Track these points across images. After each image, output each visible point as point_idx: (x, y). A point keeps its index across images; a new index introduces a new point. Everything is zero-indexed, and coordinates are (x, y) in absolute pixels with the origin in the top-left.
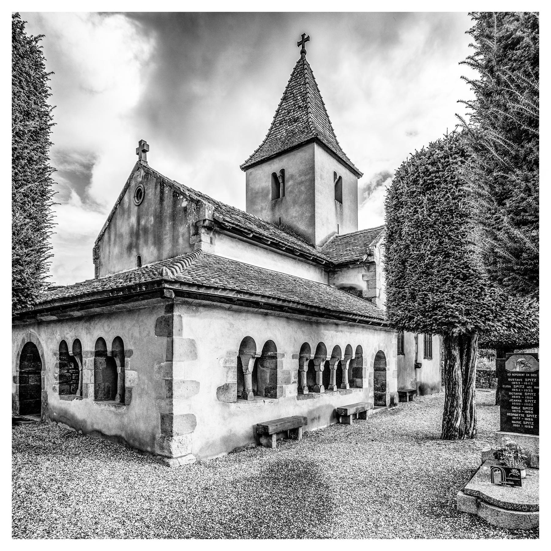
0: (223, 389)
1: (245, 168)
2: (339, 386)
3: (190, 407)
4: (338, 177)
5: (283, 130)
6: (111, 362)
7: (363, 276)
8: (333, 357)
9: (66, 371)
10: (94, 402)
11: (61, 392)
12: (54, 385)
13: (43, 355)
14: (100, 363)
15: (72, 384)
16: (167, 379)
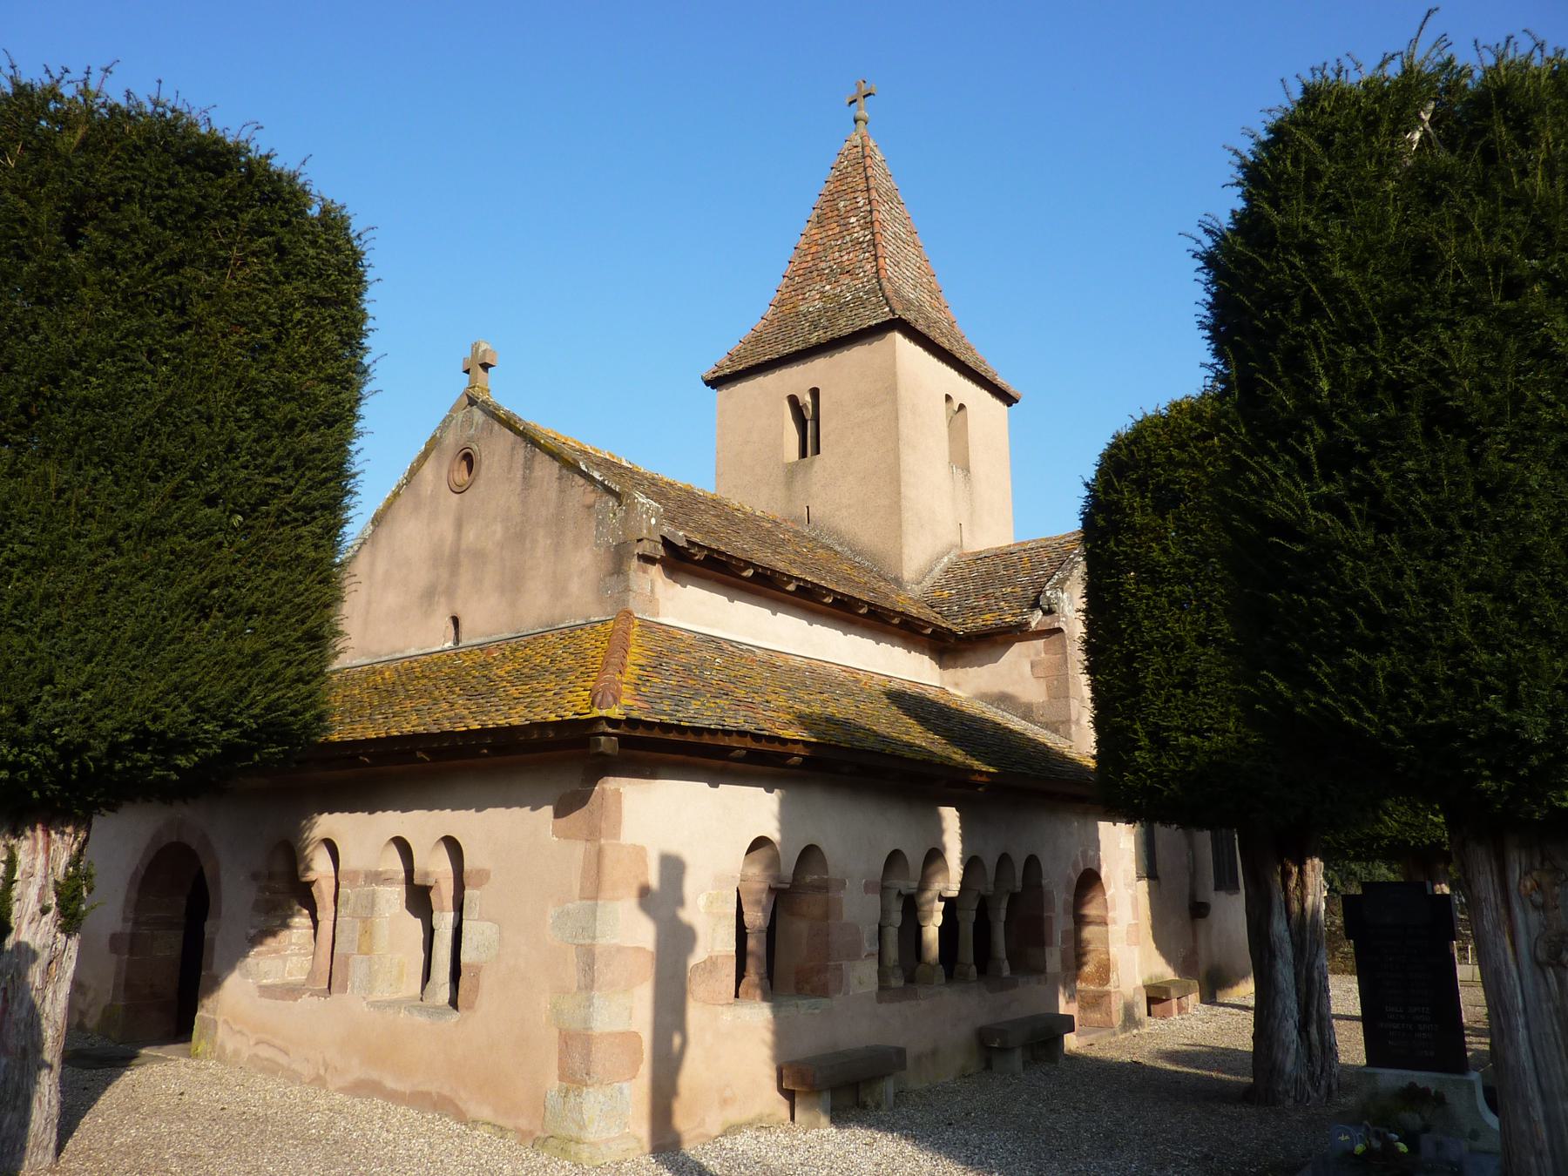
3: (631, 1012)
5: (814, 292)
9: (279, 922)
14: (388, 901)
15: (289, 955)
16: (582, 942)
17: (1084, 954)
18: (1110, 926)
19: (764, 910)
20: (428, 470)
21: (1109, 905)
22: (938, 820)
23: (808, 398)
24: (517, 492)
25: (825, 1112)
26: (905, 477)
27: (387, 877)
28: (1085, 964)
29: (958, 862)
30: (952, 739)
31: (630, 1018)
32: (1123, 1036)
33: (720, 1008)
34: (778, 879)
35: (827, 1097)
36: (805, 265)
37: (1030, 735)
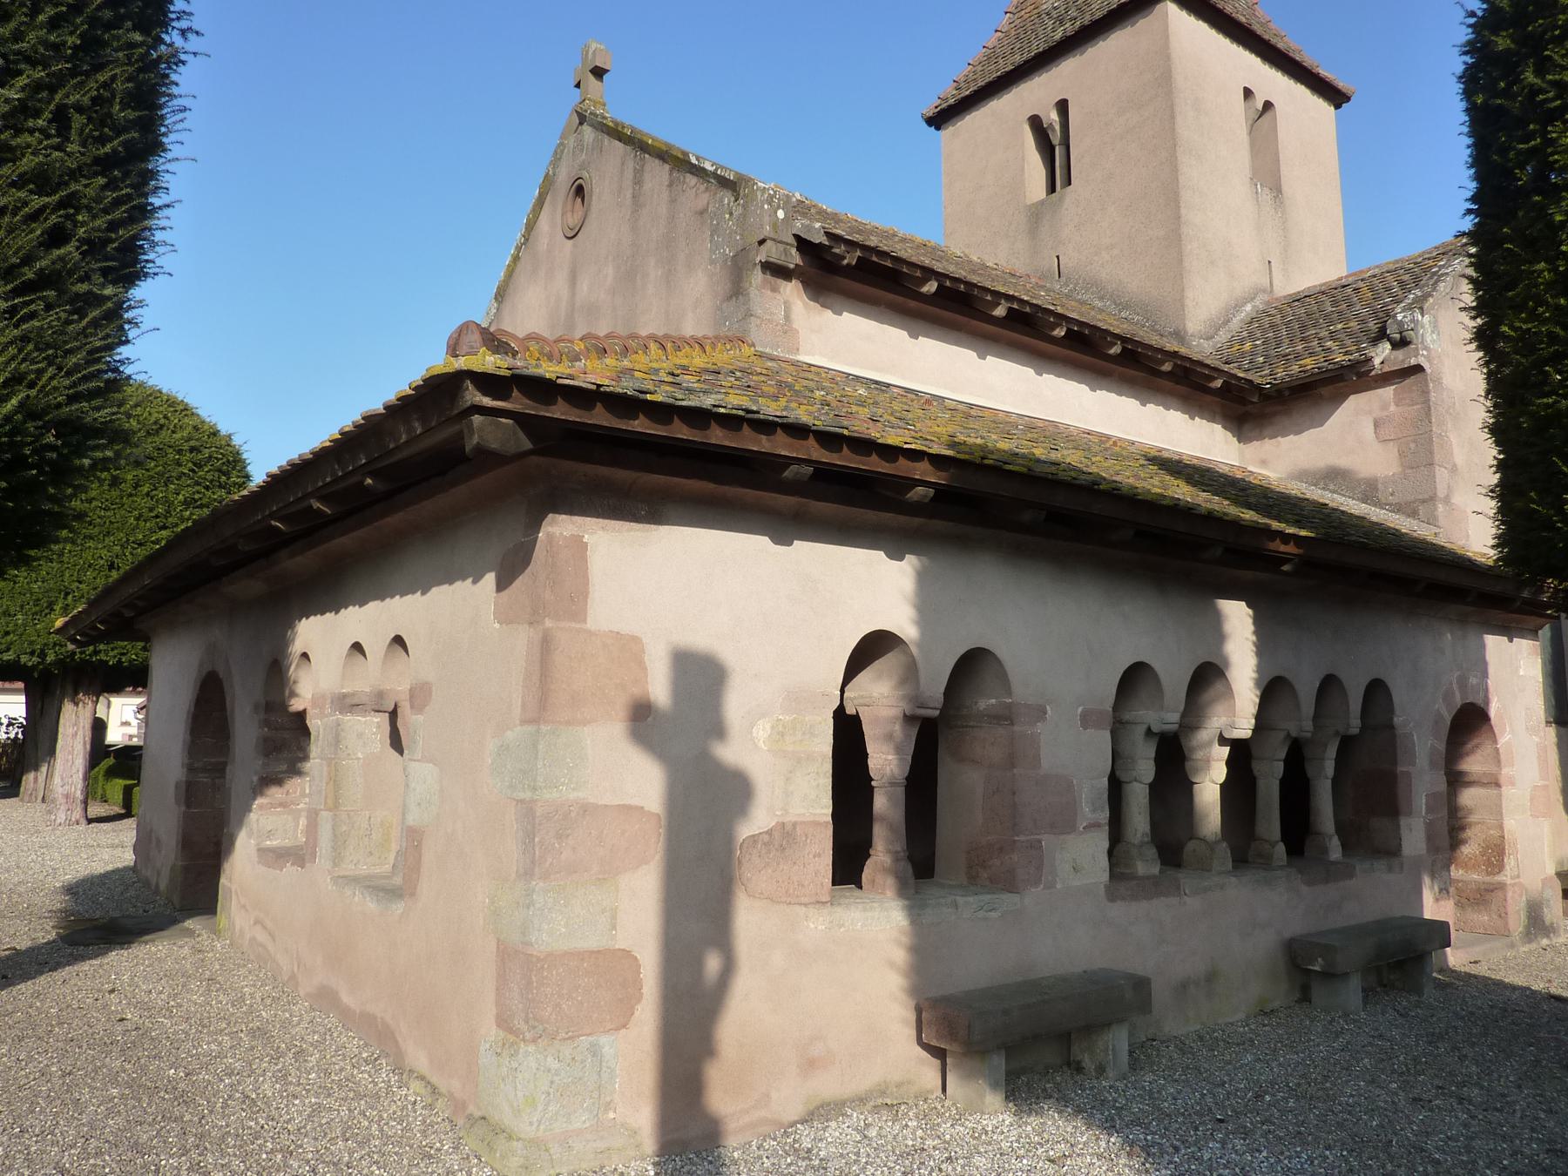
3: (614, 917)
14: (360, 735)
16: (522, 795)
17: (1463, 828)
18: (1504, 788)
19: (899, 750)
20: (544, 223)
21: (1502, 757)
22: (1217, 620)
23: (1054, 116)
24: (628, 217)
25: (994, 1086)
26: (1186, 196)
27: (356, 701)
28: (1463, 842)
29: (1251, 684)
30: (1236, 502)
31: (614, 927)
32: (1526, 948)
33: (802, 910)
34: (917, 700)
35: (999, 1061)
37: (1374, 519)
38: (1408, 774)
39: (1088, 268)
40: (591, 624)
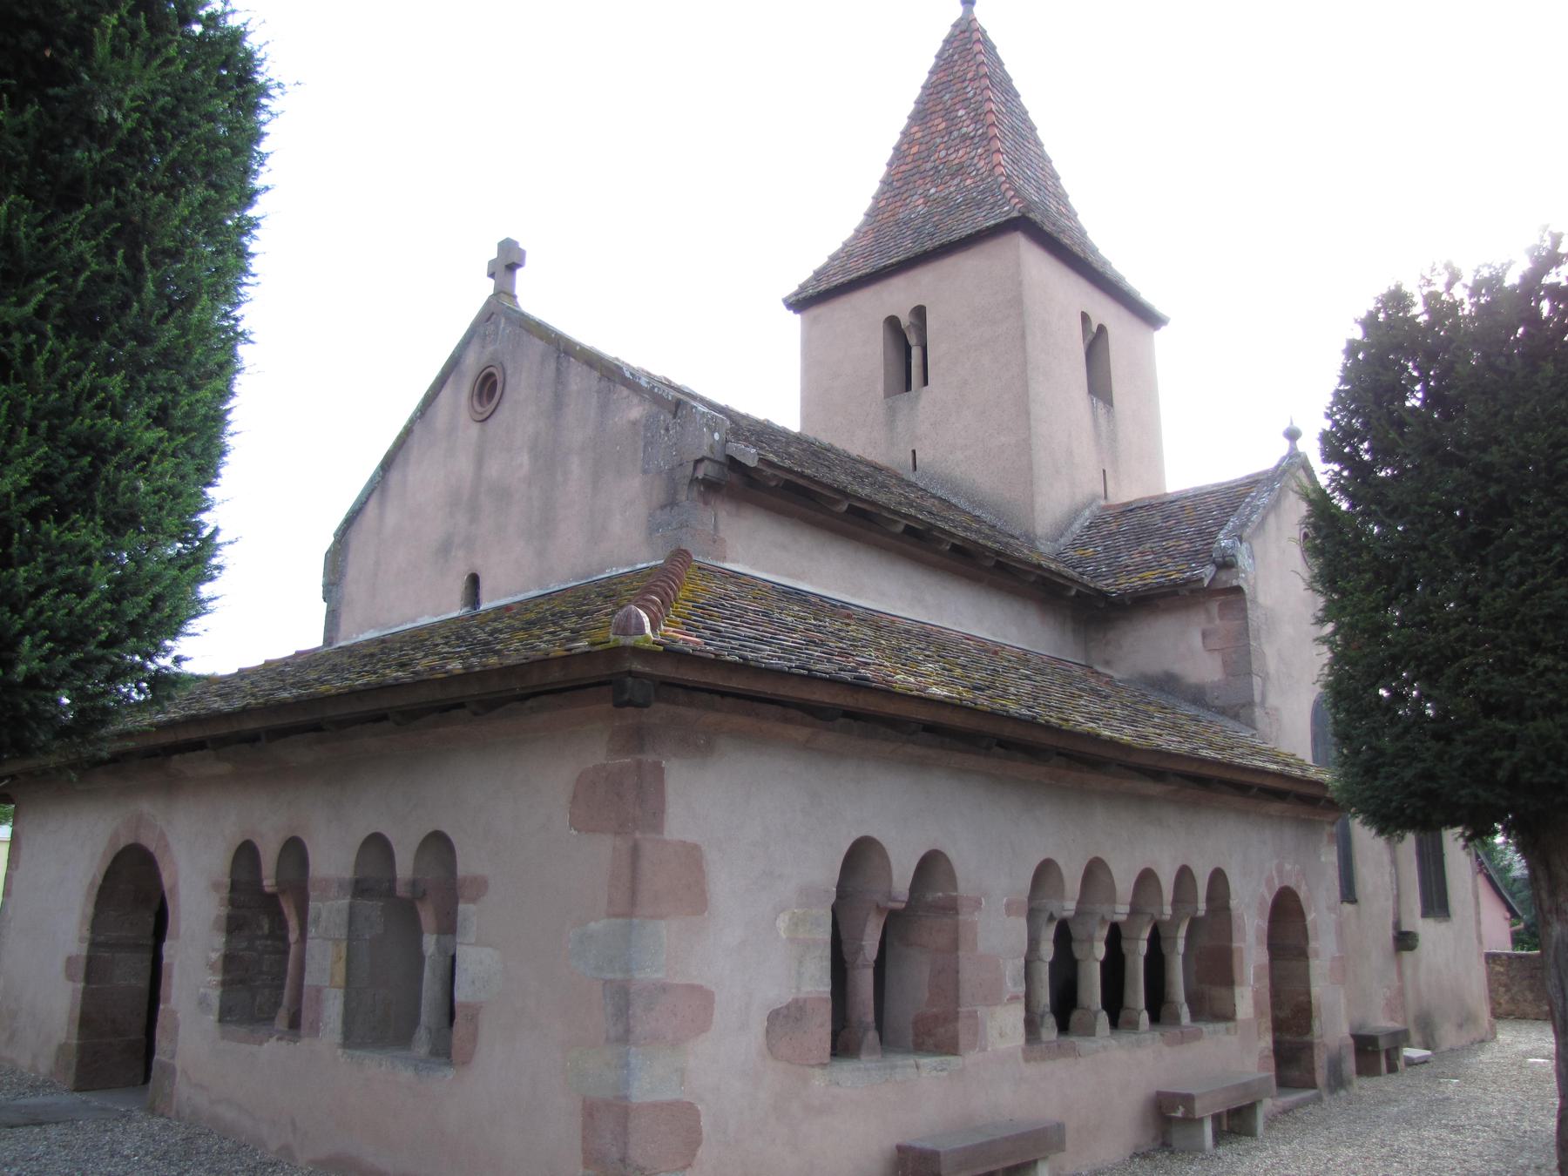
0: (784, 1019)
1: (802, 302)
2: (1155, 1018)
4: (1094, 329)
5: (916, 197)
6: (404, 913)
7: (1204, 635)
8: (1135, 911)
9: (244, 944)
10: (340, 1052)
11: (227, 1014)
12: (202, 990)
13: (174, 887)
16: (610, 976)
36: (902, 168)
38: (1241, 949)
39: (943, 465)
40: (667, 836)
